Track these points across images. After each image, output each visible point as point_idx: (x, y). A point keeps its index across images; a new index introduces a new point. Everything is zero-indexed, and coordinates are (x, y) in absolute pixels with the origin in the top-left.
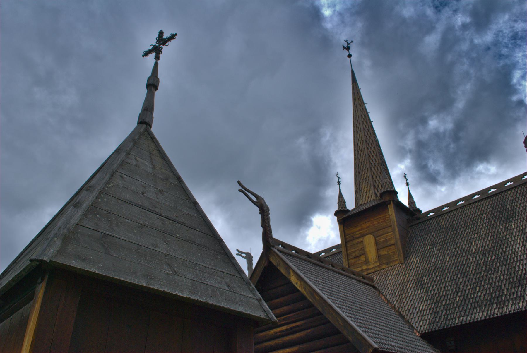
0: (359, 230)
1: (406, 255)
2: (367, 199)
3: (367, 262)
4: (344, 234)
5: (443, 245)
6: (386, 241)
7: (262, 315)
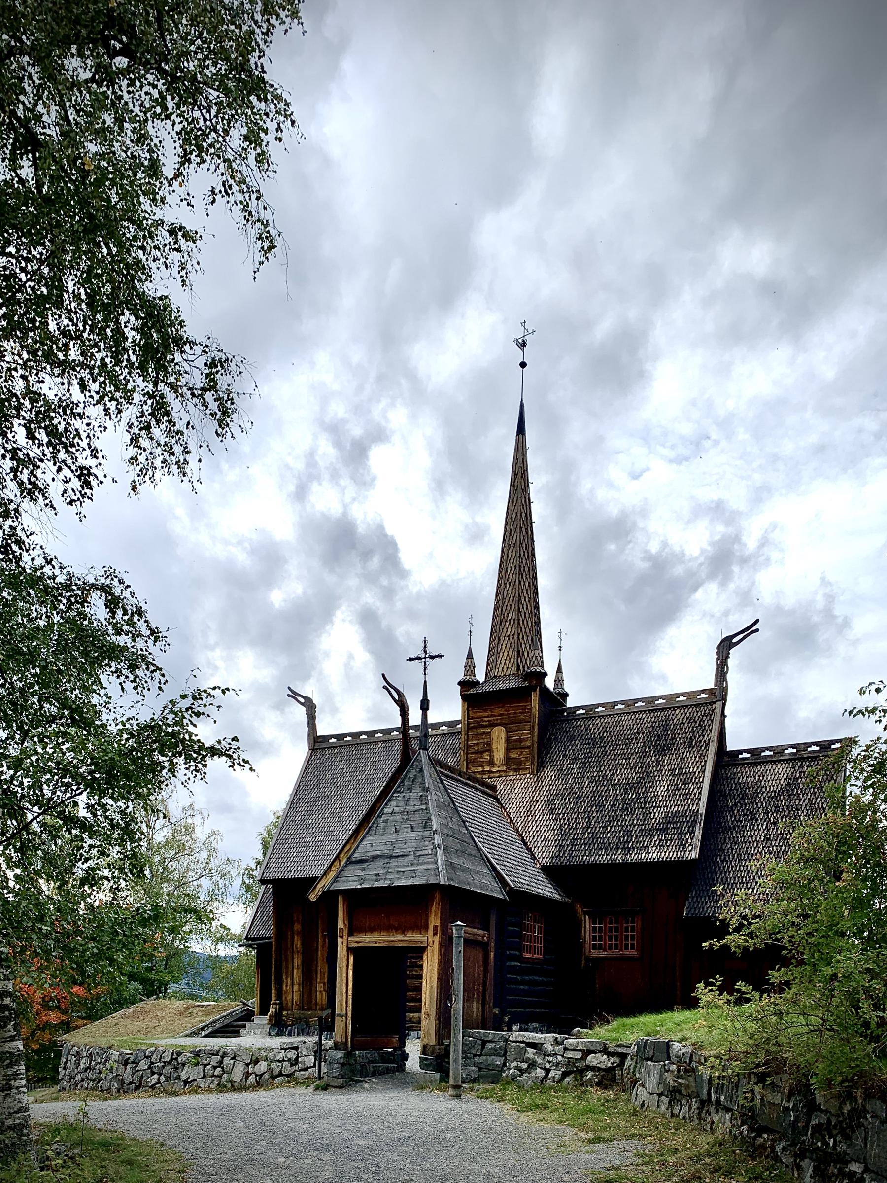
0: (488, 717)
1: (541, 766)
2: (505, 669)
3: (491, 762)
4: (467, 713)
5: (585, 763)
6: (520, 741)
7: (502, 897)
